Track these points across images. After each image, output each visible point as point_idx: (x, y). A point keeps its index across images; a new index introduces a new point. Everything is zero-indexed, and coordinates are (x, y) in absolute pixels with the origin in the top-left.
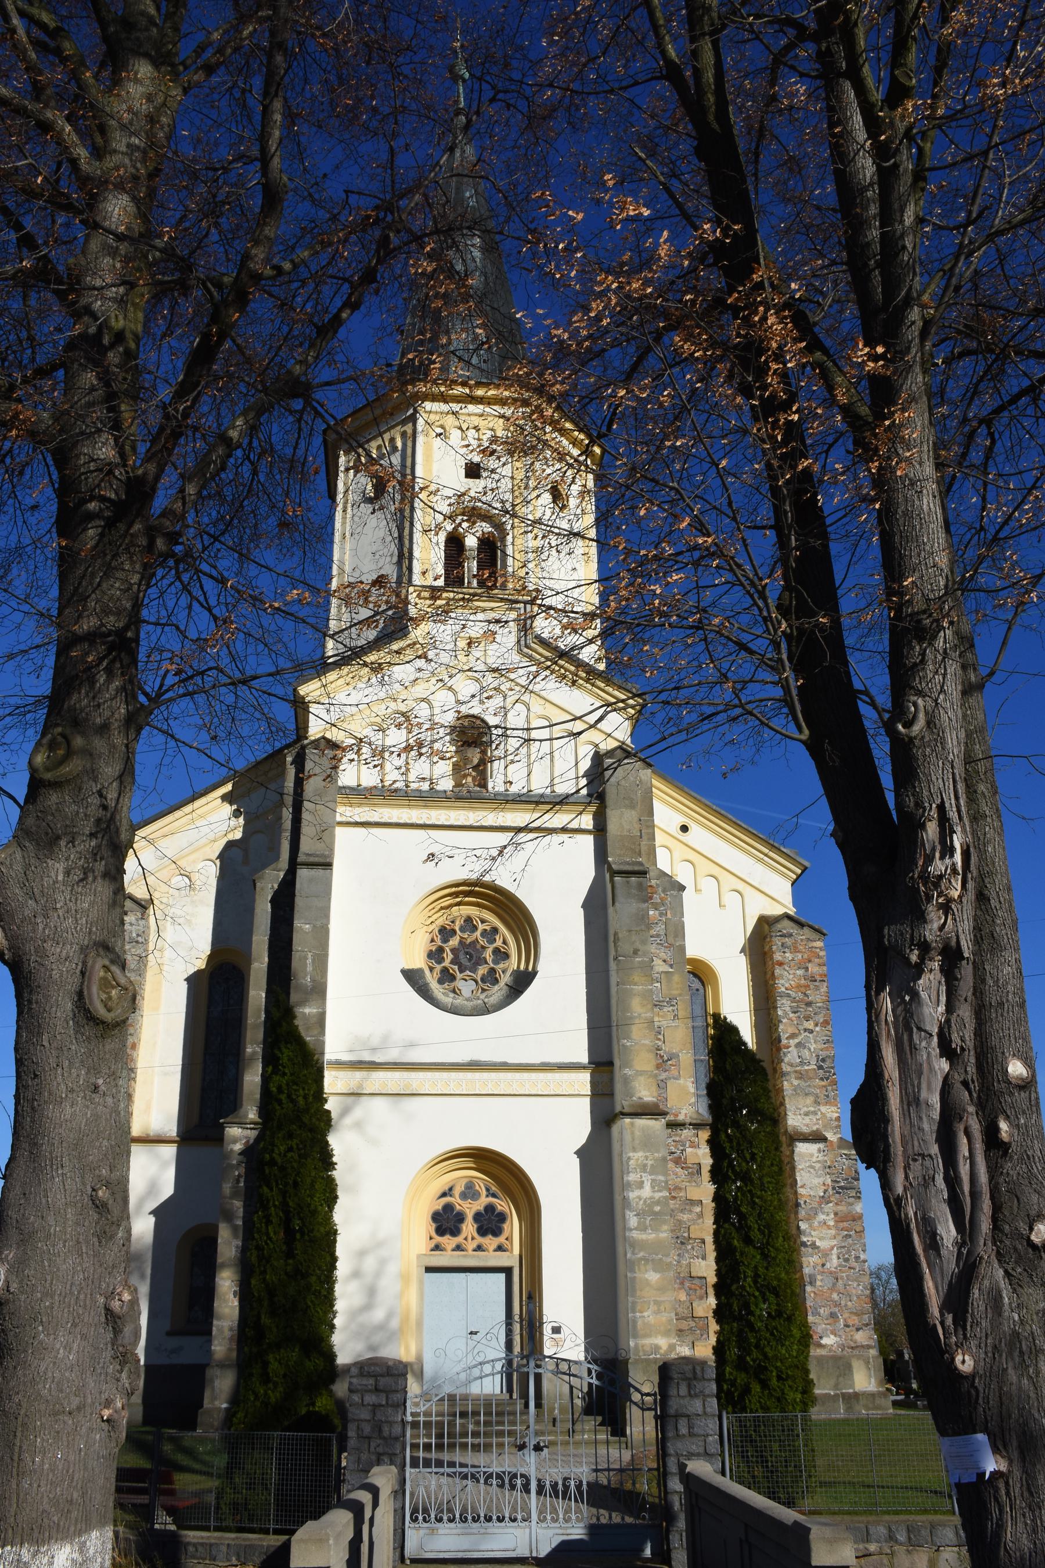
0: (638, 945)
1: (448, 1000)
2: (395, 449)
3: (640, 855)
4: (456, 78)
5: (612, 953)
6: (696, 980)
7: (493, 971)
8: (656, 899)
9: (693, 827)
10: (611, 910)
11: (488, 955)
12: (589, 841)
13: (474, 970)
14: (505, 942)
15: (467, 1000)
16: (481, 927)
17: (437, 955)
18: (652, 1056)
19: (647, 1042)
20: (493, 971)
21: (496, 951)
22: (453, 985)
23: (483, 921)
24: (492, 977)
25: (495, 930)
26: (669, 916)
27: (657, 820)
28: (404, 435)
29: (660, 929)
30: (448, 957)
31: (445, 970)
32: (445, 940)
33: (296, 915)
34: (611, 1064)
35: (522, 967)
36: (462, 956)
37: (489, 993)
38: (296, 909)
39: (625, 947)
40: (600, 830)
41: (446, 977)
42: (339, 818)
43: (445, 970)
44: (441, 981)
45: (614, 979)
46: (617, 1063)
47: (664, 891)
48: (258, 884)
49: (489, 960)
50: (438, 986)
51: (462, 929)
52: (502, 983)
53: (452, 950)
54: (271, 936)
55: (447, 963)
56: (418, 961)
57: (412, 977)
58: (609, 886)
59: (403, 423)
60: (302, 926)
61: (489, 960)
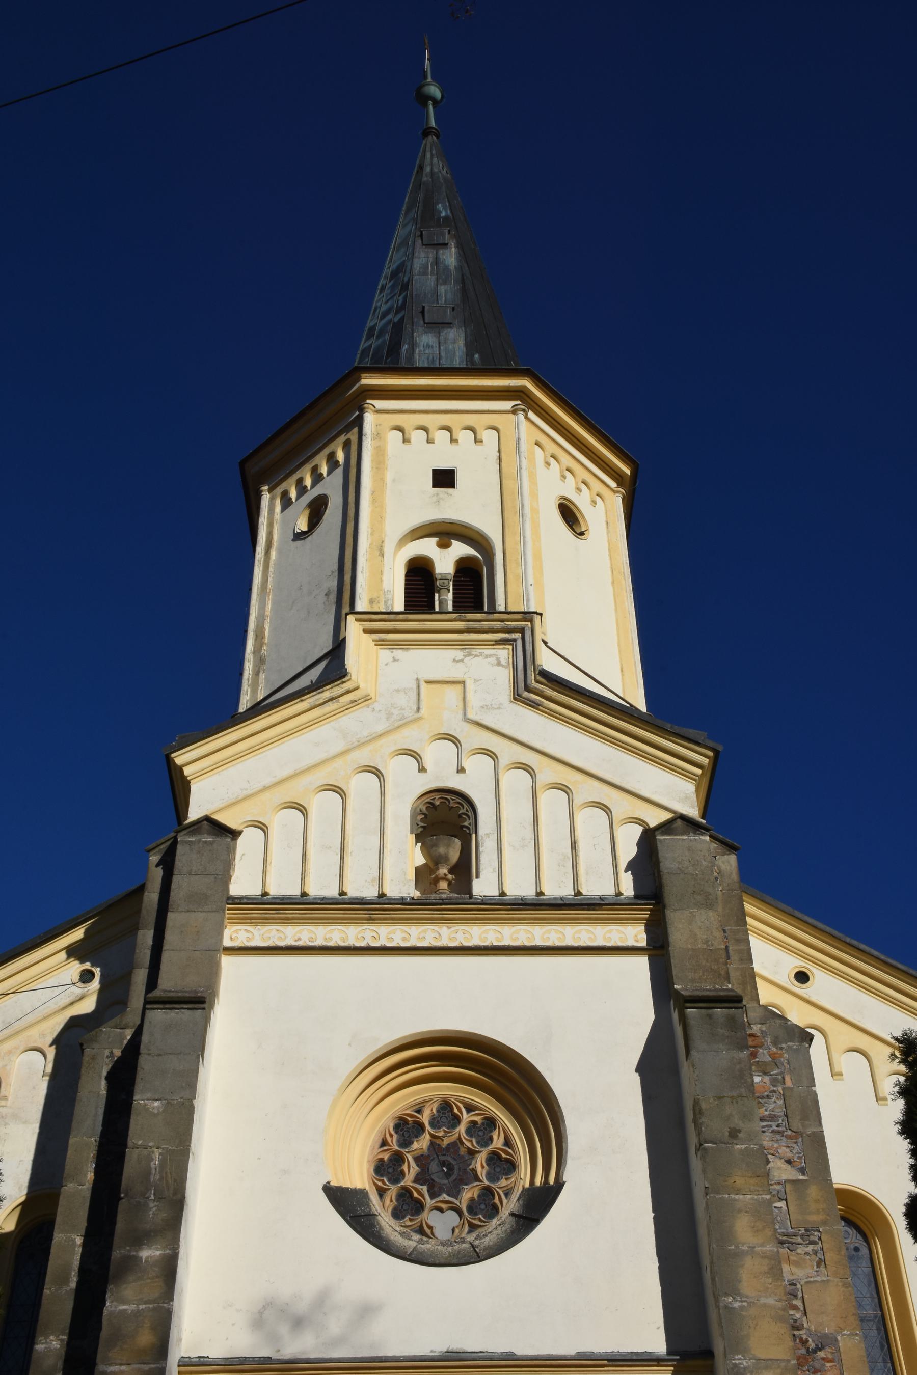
0: (737, 1122)
1: (411, 1243)
2: (336, 464)
3: (728, 979)
4: (424, 99)
5: (693, 1140)
6: (852, 1232)
7: (488, 1192)
8: (764, 1055)
9: (818, 976)
10: (685, 1069)
11: (480, 1164)
12: (642, 963)
13: (456, 1193)
14: (508, 1142)
15: (443, 1244)
16: (466, 1117)
17: (387, 1168)
18: (782, 1329)
19: (771, 1301)
20: (488, 1192)
21: (494, 1158)
22: (418, 1219)
23: (470, 1108)
24: (486, 1205)
25: (491, 1123)
26: (789, 1083)
27: (758, 966)
28: (347, 445)
29: (775, 1105)
30: (411, 1170)
31: (405, 1193)
32: (405, 1143)
33: (139, 1086)
34: (709, 1354)
35: (538, 1181)
36: (434, 1167)
37: (483, 1231)
38: (140, 1075)
39: (714, 1126)
40: (658, 949)
41: (408, 1206)
42: (227, 942)
43: (405, 1193)
44: (397, 1214)
45: (699, 1181)
46: (719, 1347)
47: (775, 1043)
48: (88, 1051)
49: (482, 1172)
50: (393, 1222)
51: (434, 1123)
52: (505, 1213)
53: (417, 1159)
54: (103, 1135)
55: (408, 1180)
56: (358, 1176)
57: (343, 1200)
58: (679, 1030)
59: (347, 429)
60: (147, 1102)
61: (482, 1172)
